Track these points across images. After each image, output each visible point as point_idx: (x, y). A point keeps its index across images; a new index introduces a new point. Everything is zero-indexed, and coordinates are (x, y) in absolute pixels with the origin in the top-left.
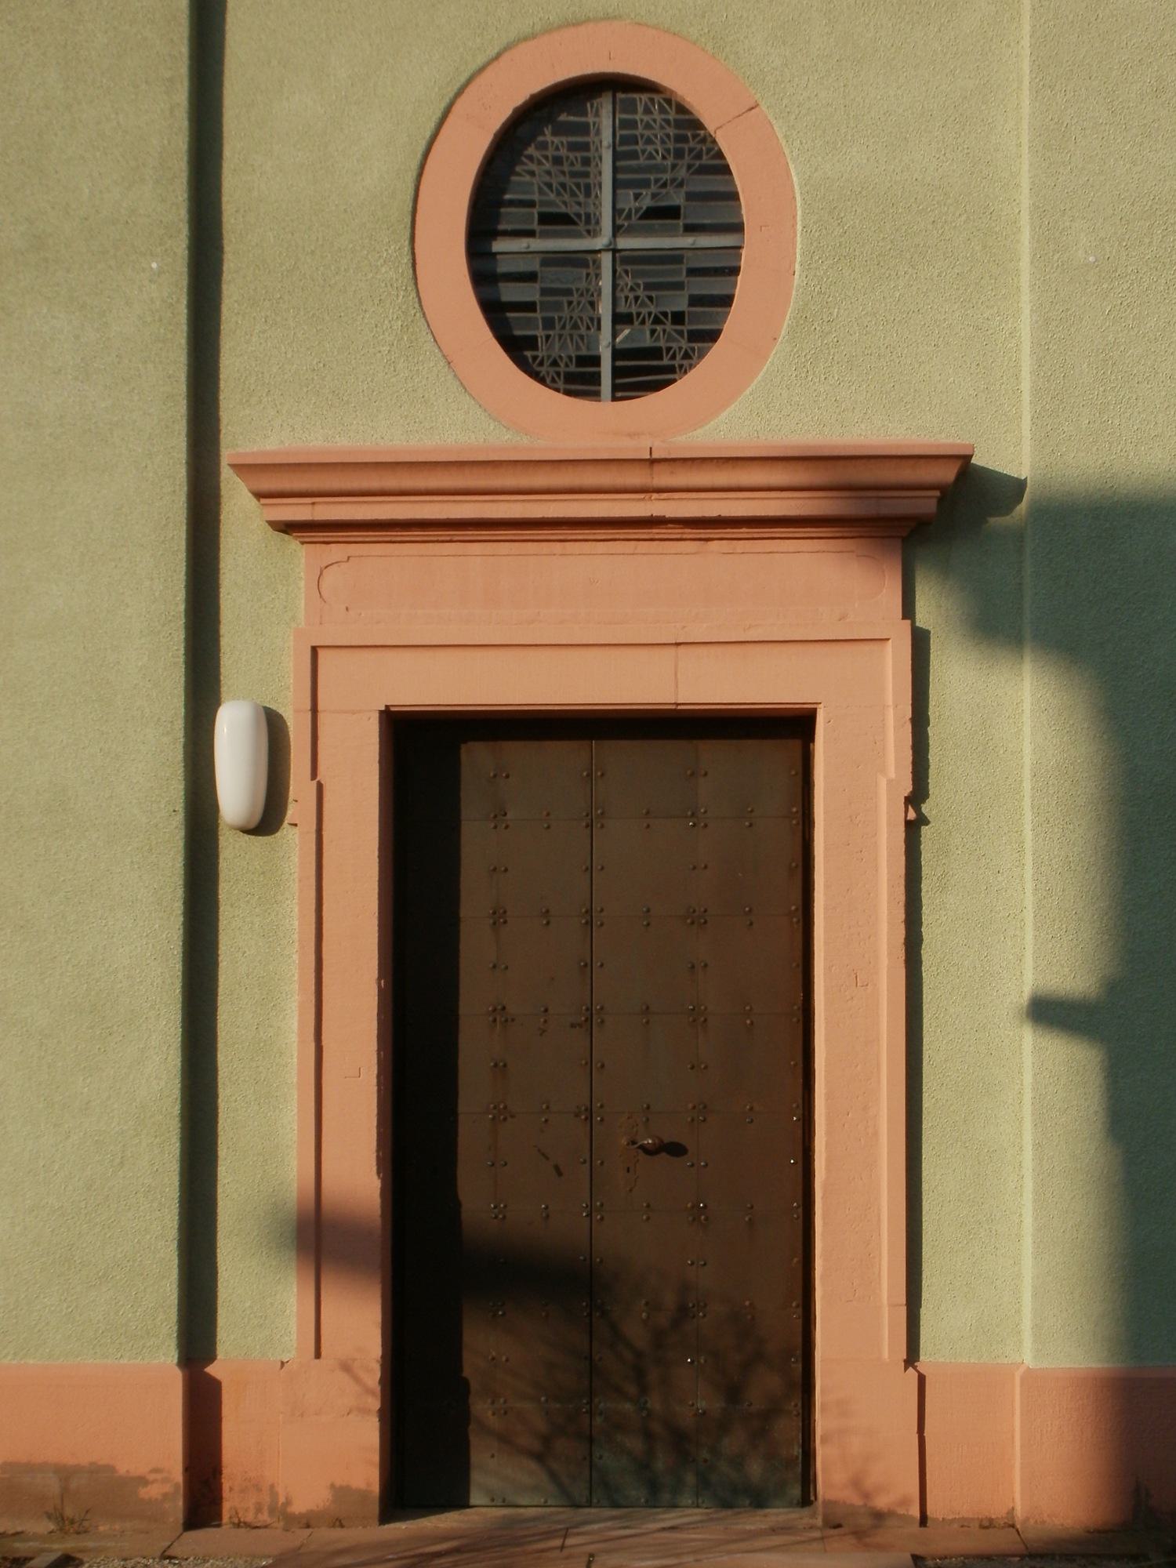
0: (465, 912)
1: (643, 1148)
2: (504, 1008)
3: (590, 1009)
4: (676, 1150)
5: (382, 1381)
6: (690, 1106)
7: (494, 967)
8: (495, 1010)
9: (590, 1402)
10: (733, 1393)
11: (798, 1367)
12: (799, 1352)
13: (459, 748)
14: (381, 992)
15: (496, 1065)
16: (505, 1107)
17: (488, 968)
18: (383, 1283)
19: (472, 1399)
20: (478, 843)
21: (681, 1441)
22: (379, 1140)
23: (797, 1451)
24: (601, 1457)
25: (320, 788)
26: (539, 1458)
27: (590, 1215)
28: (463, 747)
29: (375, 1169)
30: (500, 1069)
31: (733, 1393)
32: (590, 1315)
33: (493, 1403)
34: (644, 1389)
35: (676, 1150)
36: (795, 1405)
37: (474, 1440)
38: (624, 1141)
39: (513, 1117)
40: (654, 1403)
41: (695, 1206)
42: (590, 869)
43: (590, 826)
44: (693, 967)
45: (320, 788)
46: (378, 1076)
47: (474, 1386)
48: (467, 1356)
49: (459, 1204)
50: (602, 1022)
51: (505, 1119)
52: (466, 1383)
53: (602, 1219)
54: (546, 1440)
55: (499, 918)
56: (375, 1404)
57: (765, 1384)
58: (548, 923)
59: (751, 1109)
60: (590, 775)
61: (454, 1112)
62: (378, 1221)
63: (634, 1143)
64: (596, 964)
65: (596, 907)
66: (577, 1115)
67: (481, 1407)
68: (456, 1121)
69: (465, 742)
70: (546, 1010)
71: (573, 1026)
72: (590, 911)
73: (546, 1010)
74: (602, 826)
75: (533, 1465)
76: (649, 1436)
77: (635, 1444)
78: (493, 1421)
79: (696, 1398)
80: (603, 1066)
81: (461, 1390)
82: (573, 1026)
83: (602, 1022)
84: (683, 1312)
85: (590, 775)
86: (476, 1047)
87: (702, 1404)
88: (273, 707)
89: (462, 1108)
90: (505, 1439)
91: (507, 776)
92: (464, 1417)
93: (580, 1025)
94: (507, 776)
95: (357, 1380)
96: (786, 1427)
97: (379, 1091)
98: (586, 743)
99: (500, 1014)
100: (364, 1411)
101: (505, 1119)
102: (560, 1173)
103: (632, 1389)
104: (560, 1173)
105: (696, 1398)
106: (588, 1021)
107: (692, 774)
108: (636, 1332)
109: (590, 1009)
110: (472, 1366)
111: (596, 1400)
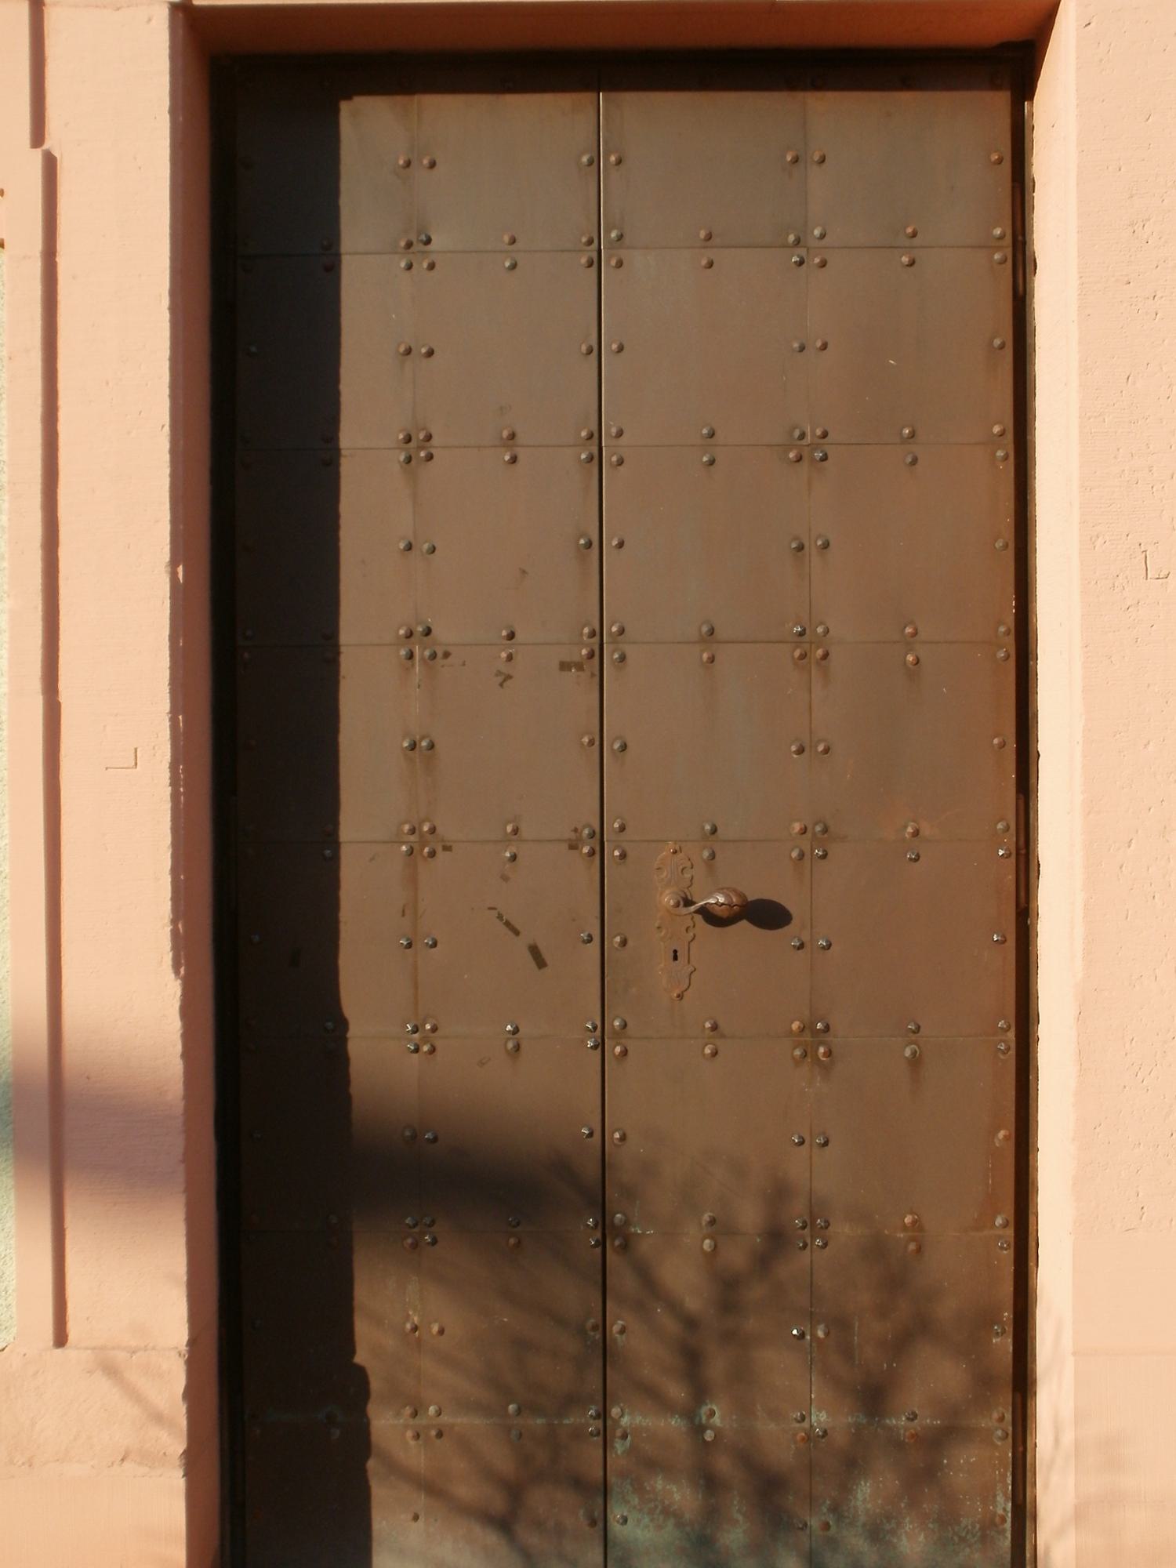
0: (349, 437)
1: (707, 914)
2: (428, 632)
3: (598, 633)
4: (768, 915)
5: (190, 1394)
6: (797, 827)
7: (409, 547)
8: (410, 635)
9: (603, 1414)
10: (873, 1397)
11: (1003, 1344)
12: (1007, 1315)
13: (336, 112)
14: (179, 595)
15: (413, 746)
16: (433, 830)
17: (399, 553)
18: (190, 1190)
19: (372, 1409)
20: (375, 302)
21: (770, 1493)
22: (175, 899)
23: (1003, 1506)
24: (625, 1521)
25: (50, 165)
26: (504, 1524)
27: (601, 1045)
28: (345, 108)
29: (168, 958)
30: (422, 751)
31: (873, 1397)
32: (602, 1243)
33: (415, 1414)
34: (700, 1392)
35: (768, 915)
36: (997, 1417)
37: (381, 1493)
38: (668, 899)
39: (447, 848)
40: (718, 1415)
41: (807, 1027)
42: (596, 351)
43: (596, 263)
44: (801, 548)
45: (50, 165)
46: (174, 767)
47: (375, 1385)
48: (362, 1328)
49: (342, 1024)
50: (623, 658)
51: (432, 854)
52: (361, 1372)
53: (625, 1052)
54: (515, 1491)
55: (417, 448)
56: (175, 1444)
57: (934, 1380)
58: (514, 460)
59: (916, 833)
60: (594, 162)
61: (332, 840)
62: (175, 1066)
63: (688, 902)
64: (610, 542)
65: (609, 428)
66: (573, 847)
67: (385, 1423)
68: (335, 859)
69: (349, 97)
70: (511, 636)
71: (565, 666)
72: (596, 436)
73: (511, 636)
74: (620, 264)
75: (492, 1538)
76: (709, 1483)
77: (681, 1495)
78: (414, 1456)
79: (798, 1405)
80: (624, 747)
81: (352, 1389)
82: (565, 666)
83: (623, 658)
84: (776, 1240)
85: (594, 162)
86: (373, 710)
87: (820, 1418)
88: (56, 154)
89: (346, 833)
90: (433, 1488)
91: (433, 165)
92: (358, 1442)
93: (580, 667)
94: (433, 165)
95: (133, 1394)
96: (973, 1465)
97: (175, 796)
98: (586, 98)
99: (419, 642)
100: (149, 1458)
101: (432, 854)
102: (541, 963)
103: (677, 1391)
104: (541, 963)
105: (798, 1405)
106: (596, 658)
107: (796, 160)
108: (684, 1277)
109: (598, 633)
110: (372, 1343)
111: (615, 1411)
